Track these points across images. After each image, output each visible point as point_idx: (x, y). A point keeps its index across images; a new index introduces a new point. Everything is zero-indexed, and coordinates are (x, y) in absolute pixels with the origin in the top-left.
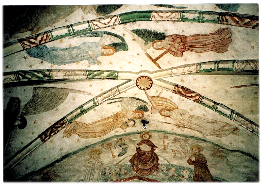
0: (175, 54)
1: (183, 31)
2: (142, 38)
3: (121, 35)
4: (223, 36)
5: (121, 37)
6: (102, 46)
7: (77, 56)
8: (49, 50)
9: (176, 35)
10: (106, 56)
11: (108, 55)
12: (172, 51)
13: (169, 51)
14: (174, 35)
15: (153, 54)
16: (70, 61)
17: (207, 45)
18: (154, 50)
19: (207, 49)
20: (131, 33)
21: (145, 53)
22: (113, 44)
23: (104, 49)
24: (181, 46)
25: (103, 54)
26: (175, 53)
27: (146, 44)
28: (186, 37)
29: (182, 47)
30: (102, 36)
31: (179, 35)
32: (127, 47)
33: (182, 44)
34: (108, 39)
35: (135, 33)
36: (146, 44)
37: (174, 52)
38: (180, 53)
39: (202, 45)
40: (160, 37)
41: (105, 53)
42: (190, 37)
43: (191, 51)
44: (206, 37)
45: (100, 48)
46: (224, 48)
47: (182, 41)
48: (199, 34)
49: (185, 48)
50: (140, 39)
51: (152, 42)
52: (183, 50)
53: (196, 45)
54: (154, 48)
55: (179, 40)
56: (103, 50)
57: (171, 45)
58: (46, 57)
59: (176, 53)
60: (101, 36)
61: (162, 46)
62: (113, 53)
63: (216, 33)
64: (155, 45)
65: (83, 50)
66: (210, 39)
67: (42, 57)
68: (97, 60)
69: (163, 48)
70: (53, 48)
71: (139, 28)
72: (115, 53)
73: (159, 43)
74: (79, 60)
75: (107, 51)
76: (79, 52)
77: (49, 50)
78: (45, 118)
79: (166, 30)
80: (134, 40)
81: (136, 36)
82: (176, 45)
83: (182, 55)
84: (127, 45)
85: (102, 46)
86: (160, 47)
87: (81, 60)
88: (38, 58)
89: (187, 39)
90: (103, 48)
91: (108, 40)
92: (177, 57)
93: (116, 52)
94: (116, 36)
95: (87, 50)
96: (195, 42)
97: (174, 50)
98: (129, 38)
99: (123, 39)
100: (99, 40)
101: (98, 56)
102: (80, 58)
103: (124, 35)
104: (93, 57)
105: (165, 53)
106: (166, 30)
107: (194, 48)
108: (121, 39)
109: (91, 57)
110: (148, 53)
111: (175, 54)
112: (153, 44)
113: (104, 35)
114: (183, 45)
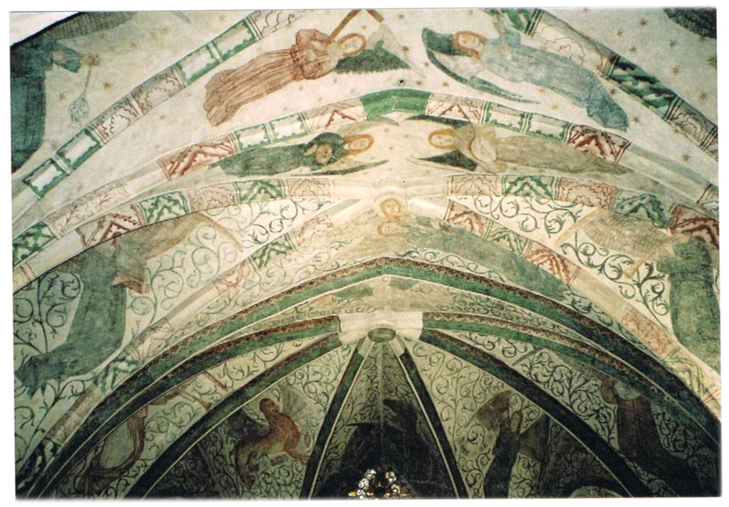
0: (314, 35)
1: (301, 88)
2: (387, 53)
3: (432, 66)
4: (223, 107)
5: (433, 62)
6: (479, 58)
7: (537, 63)
8: (586, 105)
9: (314, 78)
10: (475, 31)
11: (473, 34)
12: (322, 41)
13: (327, 41)
14: (319, 77)
15: (364, 22)
16: (558, 63)
17: (247, 80)
18: (363, 33)
19: (248, 71)
20: (410, 65)
21: (383, 22)
22: (454, 54)
23: (477, 49)
24: (302, 57)
25: (483, 41)
26: (313, 38)
27: (381, 42)
28: (294, 78)
29: (298, 55)
30: (473, 77)
31: (308, 78)
32: (425, 36)
33: (300, 62)
34: (462, 67)
35: (403, 62)
36: (381, 42)
37: (316, 40)
38: (302, 41)
39: (258, 75)
40: (349, 64)
41: (477, 41)
42: (286, 83)
43: (278, 53)
44: (255, 94)
45: (484, 57)
46: (213, 89)
47: (301, 67)
48: (268, 93)
49: (293, 52)
50: (392, 51)
51: (366, 48)
52: (297, 49)
53: (270, 71)
54: (362, 37)
55: (307, 68)
56: (479, 49)
57: (325, 53)
58: (600, 97)
59: (312, 39)
60: (475, 80)
61: (344, 44)
62: (458, 34)
63: (235, 109)
64: (359, 44)
65: (521, 67)
66: (246, 93)
67: (607, 99)
68: (499, 32)
69: (341, 42)
70: (578, 102)
71: (394, 71)
72: (454, 33)
73: (350, 50)
74: (539, 53)
75: (470, 44)
76: (532, 69)
77: (586, 105)
78: (553, 285)
79: (335, 81)
80: (406, 49)
81: (401, 56)
82: (313, 57)
83: (298, 36)
84: (423, 40)
85: (479, 58)
86: (349, 41)
87: (535, 50)
88: (615, 104)
89: (290, 77)
90: (477, 53)
91: (463, 64)
92: (309, 28)
93: (451, 35)
94: (444, 68)
95: (514, 64)
96: (274, 75)
97: (317, 45)
98: (418, 53)
99: (431, 55)
100: (481, 73)
101: (495, 43)
102: (534, 55)
103: (427, 64)
104: (504, 43)
105: (337, 31)
106: (335, 81)
107: (273, 60)
108: (434, 58)
109: (510, 45)
110: (378, 23)
111: (315, 35)
112: (364, 46)
113: (468, 78)
114: (298, 60)
